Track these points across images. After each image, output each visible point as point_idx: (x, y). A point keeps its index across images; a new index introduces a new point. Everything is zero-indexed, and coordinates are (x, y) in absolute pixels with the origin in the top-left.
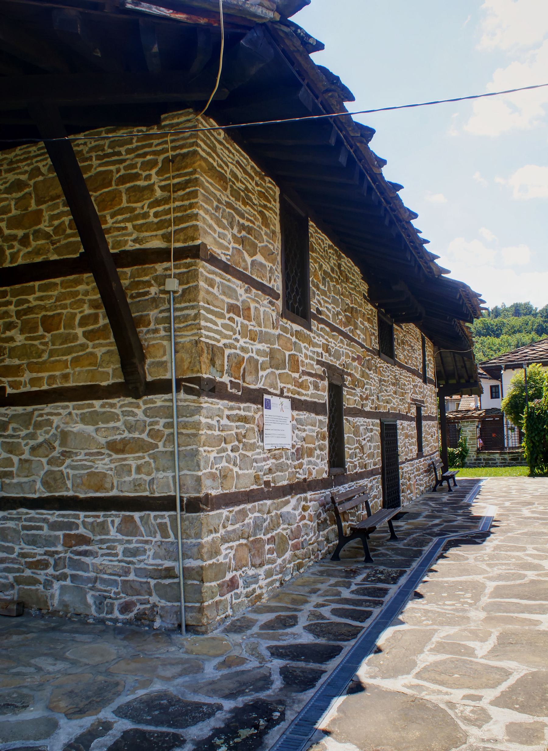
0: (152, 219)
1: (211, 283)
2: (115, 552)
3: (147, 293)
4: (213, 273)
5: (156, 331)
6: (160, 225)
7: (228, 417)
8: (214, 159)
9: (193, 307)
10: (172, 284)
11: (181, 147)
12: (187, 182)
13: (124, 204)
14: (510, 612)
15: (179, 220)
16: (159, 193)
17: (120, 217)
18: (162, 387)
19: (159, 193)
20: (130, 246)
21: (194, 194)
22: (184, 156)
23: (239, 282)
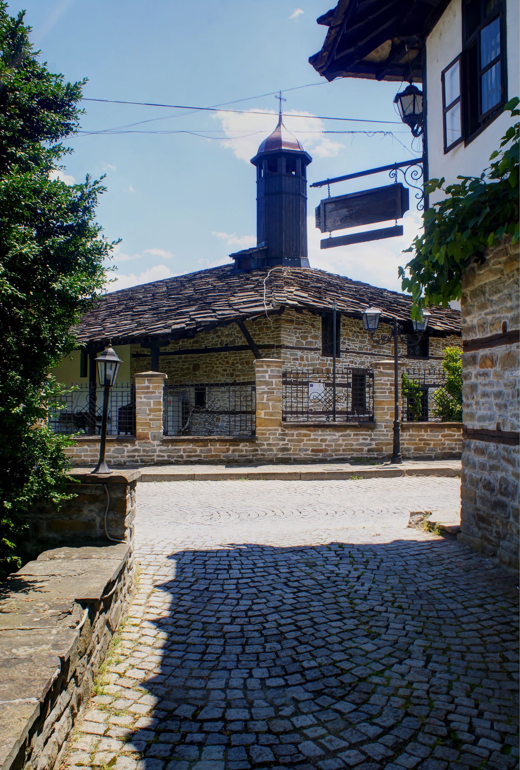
6: (273, 338)
20: (266, 343)
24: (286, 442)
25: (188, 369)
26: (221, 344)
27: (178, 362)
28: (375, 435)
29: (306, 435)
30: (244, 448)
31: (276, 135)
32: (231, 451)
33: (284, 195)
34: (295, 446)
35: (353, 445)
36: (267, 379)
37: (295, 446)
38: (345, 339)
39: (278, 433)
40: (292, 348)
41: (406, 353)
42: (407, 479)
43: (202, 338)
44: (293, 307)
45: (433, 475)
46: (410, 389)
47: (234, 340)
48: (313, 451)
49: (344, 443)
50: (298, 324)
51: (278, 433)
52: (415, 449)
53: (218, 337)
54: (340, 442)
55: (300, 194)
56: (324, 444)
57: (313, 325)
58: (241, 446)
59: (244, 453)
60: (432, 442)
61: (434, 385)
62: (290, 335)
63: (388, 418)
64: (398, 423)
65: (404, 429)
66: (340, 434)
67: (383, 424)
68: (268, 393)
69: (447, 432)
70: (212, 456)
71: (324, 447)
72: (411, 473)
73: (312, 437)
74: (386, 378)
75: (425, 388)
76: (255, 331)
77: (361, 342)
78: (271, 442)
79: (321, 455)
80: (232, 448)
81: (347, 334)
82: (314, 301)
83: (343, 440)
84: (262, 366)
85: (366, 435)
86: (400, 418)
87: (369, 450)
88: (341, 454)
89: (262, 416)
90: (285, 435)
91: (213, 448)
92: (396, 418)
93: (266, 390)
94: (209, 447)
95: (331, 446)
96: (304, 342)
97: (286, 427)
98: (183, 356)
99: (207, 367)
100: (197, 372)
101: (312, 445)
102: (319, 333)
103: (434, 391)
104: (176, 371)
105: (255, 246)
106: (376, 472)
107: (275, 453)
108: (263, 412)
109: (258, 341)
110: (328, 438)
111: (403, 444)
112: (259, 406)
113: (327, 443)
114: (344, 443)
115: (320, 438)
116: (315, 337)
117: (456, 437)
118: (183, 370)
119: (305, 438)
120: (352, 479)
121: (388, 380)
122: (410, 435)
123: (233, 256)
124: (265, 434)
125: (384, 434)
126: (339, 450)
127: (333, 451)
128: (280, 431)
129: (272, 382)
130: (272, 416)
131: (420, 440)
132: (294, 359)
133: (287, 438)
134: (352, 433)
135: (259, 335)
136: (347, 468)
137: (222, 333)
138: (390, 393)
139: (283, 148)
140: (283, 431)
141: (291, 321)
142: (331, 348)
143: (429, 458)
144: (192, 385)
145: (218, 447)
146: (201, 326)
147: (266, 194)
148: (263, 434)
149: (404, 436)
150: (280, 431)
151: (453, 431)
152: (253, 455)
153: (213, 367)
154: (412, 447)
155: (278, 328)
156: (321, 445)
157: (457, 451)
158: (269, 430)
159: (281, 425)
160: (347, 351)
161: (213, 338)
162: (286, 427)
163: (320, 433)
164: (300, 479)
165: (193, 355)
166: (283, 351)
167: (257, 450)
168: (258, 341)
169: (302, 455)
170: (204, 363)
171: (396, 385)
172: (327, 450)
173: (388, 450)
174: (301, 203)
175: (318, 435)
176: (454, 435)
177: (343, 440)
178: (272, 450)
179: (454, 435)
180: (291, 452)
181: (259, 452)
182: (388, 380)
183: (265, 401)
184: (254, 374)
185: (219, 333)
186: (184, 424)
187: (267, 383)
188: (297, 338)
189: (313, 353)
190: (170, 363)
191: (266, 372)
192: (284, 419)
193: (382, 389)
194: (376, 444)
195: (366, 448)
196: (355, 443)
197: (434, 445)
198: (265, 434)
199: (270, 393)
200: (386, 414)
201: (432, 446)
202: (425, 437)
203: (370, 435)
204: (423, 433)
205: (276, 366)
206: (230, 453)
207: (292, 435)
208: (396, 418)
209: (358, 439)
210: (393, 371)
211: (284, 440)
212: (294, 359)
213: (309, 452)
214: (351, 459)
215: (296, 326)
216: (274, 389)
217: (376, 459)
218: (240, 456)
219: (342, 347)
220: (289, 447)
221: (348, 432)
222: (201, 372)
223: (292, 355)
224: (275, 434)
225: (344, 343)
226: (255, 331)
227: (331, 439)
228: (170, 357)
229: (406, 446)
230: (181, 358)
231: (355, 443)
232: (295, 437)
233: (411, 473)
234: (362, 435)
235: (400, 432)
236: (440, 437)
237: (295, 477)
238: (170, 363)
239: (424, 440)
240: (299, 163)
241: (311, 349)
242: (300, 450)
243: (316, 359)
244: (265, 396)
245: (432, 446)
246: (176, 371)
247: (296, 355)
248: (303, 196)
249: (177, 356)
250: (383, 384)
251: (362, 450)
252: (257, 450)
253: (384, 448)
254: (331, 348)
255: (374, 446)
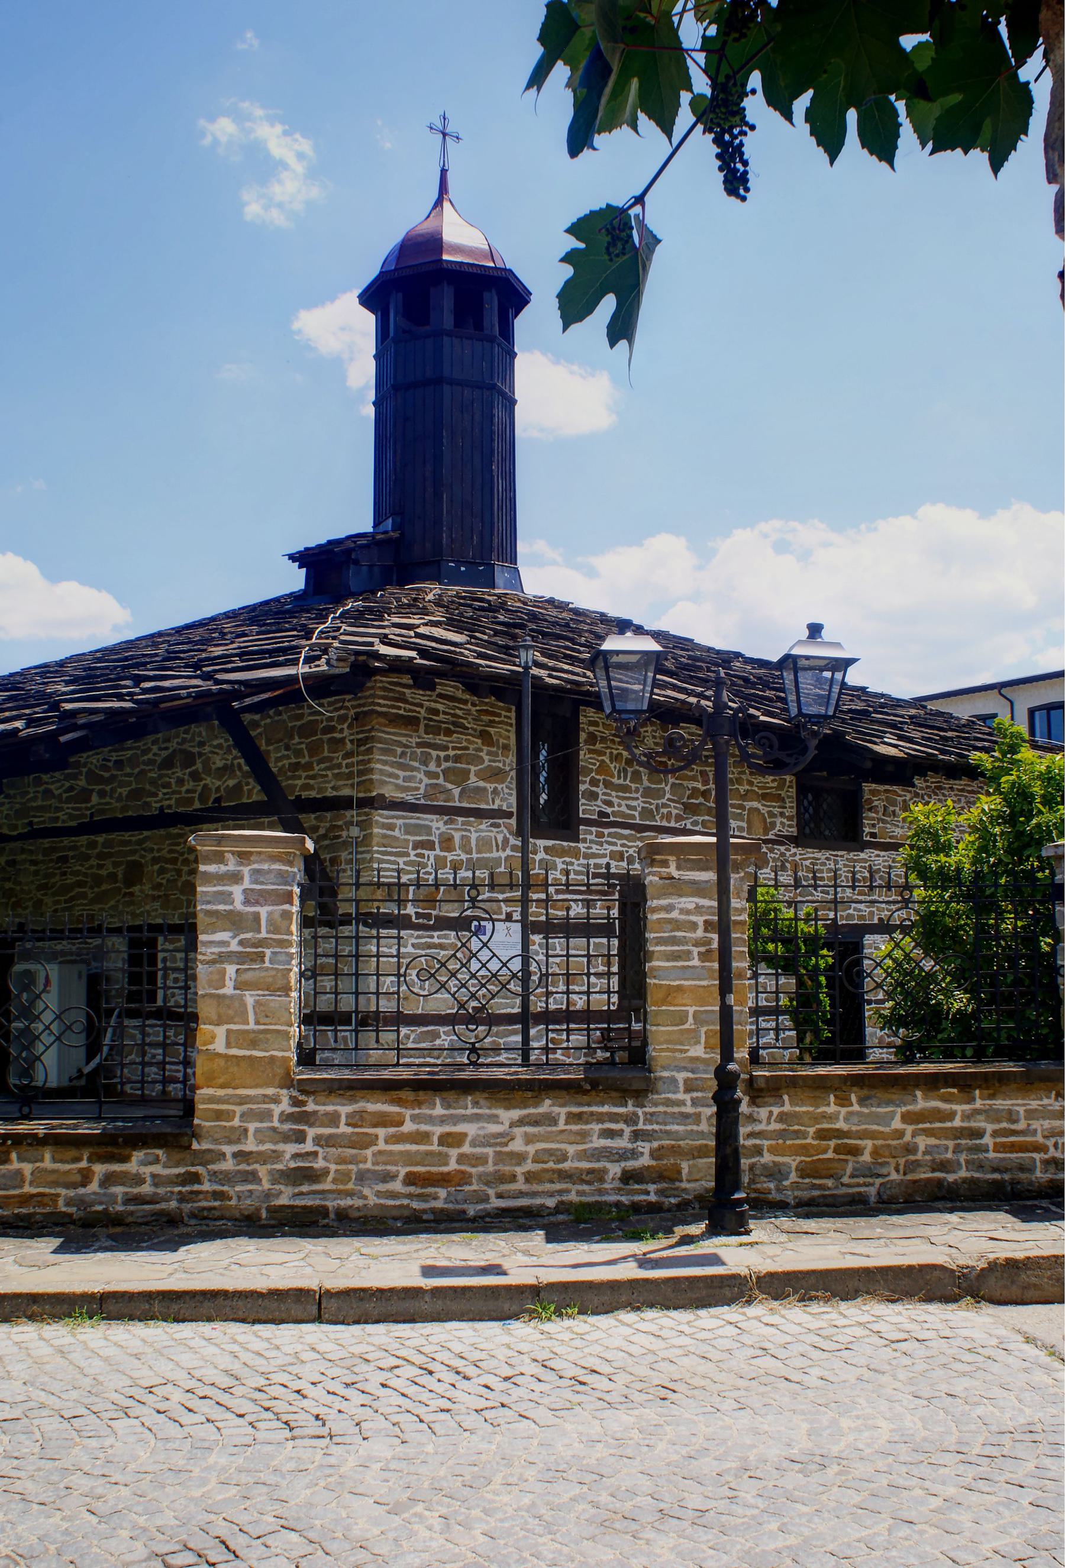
0: (344, 770)
1: (391, 827)
2: (999, 1140)
3: (340, 836)
4: (393, 817)
5: (344, 871)
6: (350, 776)
7: (413, 945)
8: (399, 708)
9: (368, 852)
10: (355, 831)
11: (363, 705)
12: (367, 738)
13: (326, 754)
14: (821, 1177)
15: (361, 773)
16: (349, 746)
17: (323, 766)
18: (346, 920)
19: (349, 746)
20: (330, 793)
21: (370, 751)
22: (365, 713)
23: (434, 817)
24: (309, 1146)
25: (112, 877)
26: (203, 798)
27: (88, 858)
28: (650, 1118)
29: (383, 1120)
30: (148, 1169)
31: (428, 227)
32: (101, 1184)
33: (447, 389)
34: (341, 1161)
35: (564, 1158)
36: (238, 905)
37: (341, 1161)
38: (594, 782)
39: (277, 1110)
40: (413, 808)
41: (794, 831)
42: (758, 1318)
43: (153, 782)
44: (397, 666)
45: (1055, 82)
46: (784, 942)
47: (238, 787)
48: (411, 1179)
49: (531, 1149)
50: (434, 729)
51: (277, 1110)
52: (803, 1172)
53: (195, 776)
54: (517, 1146)
55: (493, 387)
56: (454, 1153)
57: (485, 737)
58: (136, 1163)
59: (147, 1189)
60: (868, 1144)
61: (884, 928)
62: (403, 767)
63: (698, 1051)
64: (735, 1076)
65: (758, 1093)
66: (516, 1114)
67: (681, 1076)
68: (239, 958)
69: (922, 1102)
70: (25, 1200)
71: (453, 1166)
72: (784, 1286)
73: (408, 1127)
74: (689, 902)
75: (847, 943)
76: (299, 753)
77: (648, 793)
78: (250, 1145)
79: (441, 1198)
80: (100, 1169)
81: (603, 769)
82: (481, 656)
83: (529, 1140)
84: (219, 858)
85: (614, 1118)
86: (742, 1053)
87: (628, 1177)
88: (520, 1193)
89: (219, 1046)
90: (305, 1118)
91: (27, 1168)
92: (727, 1054)
93: (234, 946)
94: (15, 1165)
95: (481, 1160)
96: (456, 792)
97: (306, 1088)
98: (100, 839)
99: (162, 871)
100: (136, 889)
101: (408, 1158)
102: (509, 761)
103: (877, 946)
104: (80, 884)
105: (366, 525)
106: (633, 1283)
107: (268, 1189)
108: (221, 1031)
109: (306, 787)
110: (471, 1129)
111: (758, 1151)
112: (205, 1009)
113: (466, 1149)
114: (531, 1149)
115: (438, 1130)
116: (495, 775)
117: (957, 1123)
118: (98, 880)
119: (381, 1132)
120: (534, 1315)
121: (699, 909)
122: (782, 1118)
123: (302, 558)
124: (229, 1116)
125: (681, 1109)
126: (513, 1178)
127: (488, 1180)
128: (285, 1106)
129: (257, 917)
130: (254, 1044)
131: (823, 1135)
132: (417, 845)
133: (311, 1132)
134: (562, 1112)
135: (309, 766)
136: (528, 1259)
137: (206, 764)
138: (704, 956)
139: (445, 257)
140: (296, 1102)
141: (411, 722)
142: (554, 812)
143: (855, 1206)
144: (118, 931)
145: (48, 1163)
146: (75, 728)
147: (396, 388)
148: (219, 1115)
149: (760, 1122)
150: (285, 1106)
151: (946, 1099)
152: (182, 1198)
153: (179, 872)
154: (792, 1162)
155: (364, 743)
156: (444, 1159)
157: (963, 1173)
158: (243, 1100)
159: (288, 1083)
160: (602, 821)
161: (180, 782)
162: (306, 1088)
163: (439, 1110)
164: (319, 1319)
165: (126, 836)
166: (380, 817)
167: (195, 1178)
168: (306, 787)
169: (371, 1197)
170: (155, 860)
171: (723, 926)
172: (464, 1178)
173: (698, 1176)
174: (498, 412)
175: (431, 1120)
176: (951, 1116)
177: (529, 1140)
178: (252, 1177)
179: (951, 1116)
180: (327, 1185)
181: (206, 1187)
182: (699, 909)
183: (228, 990)
184: (191, 888)
185: (199, 766)
186: (92, 1049)
187: (235, 921)
188: (428, 774)
189: (485, 824)
190: (64, 859)
191: (235, 878)
192: (307, 1058)
193: (674, 941)
194: (655, 1154)
195: (615, 1170)
196: (571, 1149)
197: (875, 1152)
198: (229, 1116)
199: (250, 956)
200: (692, 1037)
201: (866, 1157)
202: (841, 1125)
203: (630, 1119)
204: (832, 1109)
205: (274, 859)
206: (94, 1187)
207: (333, 1119)
208: (727, 1054)
209: (584, 1136)
210: (710, 876)
211: (300, 1137)
212: (417, 845)
213: (397, 1186)
214: (558, 1209)
215: (429, 738)
216: (261, 943)
217: (654, 1208)
218: (130, 1200)
219: (586, 808)
220: (320, 1164)
221: (547, 1106)
222: (147, 888)
223: (409, 829)
224: (267, 1115)
225: (594, 796)
226: (299, 753)
227: (486, 1136)
228: (66, 841)
229: (767, 1158)
230: (92, 845)
231: (571, 1149)
232: (343, 1129)
233: (784, 1286)
234: (600, 1118)
235: (744, 1108)
236: (897, 1124)
237: (296, 1310)
238: (64, 859)
239: (839, 1134)
240: (491, 302)
241: (479, 814)
242: (362, 1177)
243: (492, 844)
244: (231, 970)
245: (866, 1157)
246: (80, 884)
247: (428, 830)
248: (503, 394)
249: (83, 839)
250: (677, 925)
251: (599, 1175)
252: (195, 1178)
253: (685, 1166)
254: (554, 812)
255: (645, 1161)
